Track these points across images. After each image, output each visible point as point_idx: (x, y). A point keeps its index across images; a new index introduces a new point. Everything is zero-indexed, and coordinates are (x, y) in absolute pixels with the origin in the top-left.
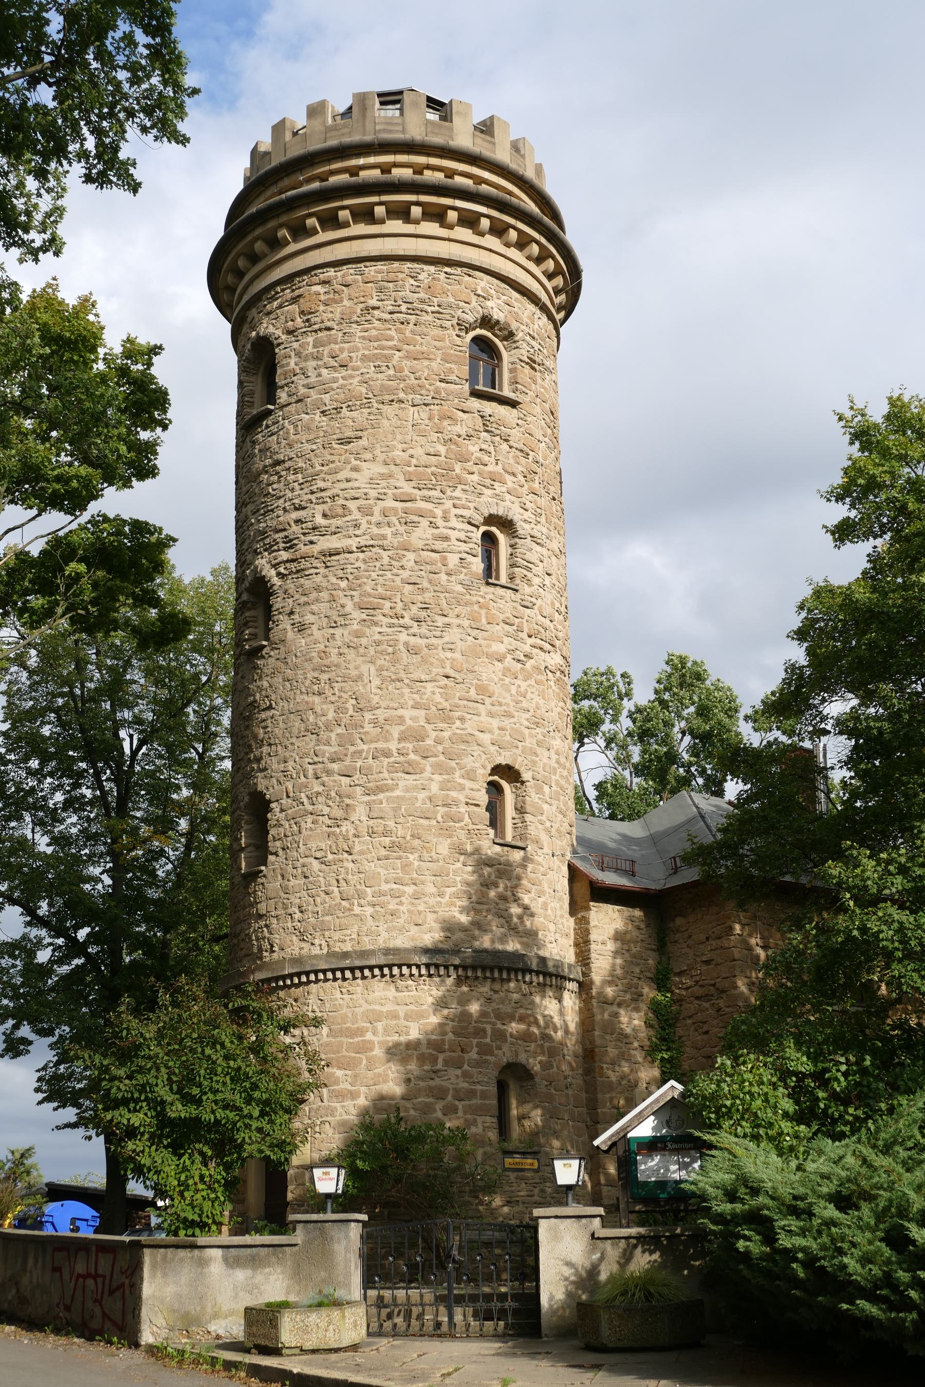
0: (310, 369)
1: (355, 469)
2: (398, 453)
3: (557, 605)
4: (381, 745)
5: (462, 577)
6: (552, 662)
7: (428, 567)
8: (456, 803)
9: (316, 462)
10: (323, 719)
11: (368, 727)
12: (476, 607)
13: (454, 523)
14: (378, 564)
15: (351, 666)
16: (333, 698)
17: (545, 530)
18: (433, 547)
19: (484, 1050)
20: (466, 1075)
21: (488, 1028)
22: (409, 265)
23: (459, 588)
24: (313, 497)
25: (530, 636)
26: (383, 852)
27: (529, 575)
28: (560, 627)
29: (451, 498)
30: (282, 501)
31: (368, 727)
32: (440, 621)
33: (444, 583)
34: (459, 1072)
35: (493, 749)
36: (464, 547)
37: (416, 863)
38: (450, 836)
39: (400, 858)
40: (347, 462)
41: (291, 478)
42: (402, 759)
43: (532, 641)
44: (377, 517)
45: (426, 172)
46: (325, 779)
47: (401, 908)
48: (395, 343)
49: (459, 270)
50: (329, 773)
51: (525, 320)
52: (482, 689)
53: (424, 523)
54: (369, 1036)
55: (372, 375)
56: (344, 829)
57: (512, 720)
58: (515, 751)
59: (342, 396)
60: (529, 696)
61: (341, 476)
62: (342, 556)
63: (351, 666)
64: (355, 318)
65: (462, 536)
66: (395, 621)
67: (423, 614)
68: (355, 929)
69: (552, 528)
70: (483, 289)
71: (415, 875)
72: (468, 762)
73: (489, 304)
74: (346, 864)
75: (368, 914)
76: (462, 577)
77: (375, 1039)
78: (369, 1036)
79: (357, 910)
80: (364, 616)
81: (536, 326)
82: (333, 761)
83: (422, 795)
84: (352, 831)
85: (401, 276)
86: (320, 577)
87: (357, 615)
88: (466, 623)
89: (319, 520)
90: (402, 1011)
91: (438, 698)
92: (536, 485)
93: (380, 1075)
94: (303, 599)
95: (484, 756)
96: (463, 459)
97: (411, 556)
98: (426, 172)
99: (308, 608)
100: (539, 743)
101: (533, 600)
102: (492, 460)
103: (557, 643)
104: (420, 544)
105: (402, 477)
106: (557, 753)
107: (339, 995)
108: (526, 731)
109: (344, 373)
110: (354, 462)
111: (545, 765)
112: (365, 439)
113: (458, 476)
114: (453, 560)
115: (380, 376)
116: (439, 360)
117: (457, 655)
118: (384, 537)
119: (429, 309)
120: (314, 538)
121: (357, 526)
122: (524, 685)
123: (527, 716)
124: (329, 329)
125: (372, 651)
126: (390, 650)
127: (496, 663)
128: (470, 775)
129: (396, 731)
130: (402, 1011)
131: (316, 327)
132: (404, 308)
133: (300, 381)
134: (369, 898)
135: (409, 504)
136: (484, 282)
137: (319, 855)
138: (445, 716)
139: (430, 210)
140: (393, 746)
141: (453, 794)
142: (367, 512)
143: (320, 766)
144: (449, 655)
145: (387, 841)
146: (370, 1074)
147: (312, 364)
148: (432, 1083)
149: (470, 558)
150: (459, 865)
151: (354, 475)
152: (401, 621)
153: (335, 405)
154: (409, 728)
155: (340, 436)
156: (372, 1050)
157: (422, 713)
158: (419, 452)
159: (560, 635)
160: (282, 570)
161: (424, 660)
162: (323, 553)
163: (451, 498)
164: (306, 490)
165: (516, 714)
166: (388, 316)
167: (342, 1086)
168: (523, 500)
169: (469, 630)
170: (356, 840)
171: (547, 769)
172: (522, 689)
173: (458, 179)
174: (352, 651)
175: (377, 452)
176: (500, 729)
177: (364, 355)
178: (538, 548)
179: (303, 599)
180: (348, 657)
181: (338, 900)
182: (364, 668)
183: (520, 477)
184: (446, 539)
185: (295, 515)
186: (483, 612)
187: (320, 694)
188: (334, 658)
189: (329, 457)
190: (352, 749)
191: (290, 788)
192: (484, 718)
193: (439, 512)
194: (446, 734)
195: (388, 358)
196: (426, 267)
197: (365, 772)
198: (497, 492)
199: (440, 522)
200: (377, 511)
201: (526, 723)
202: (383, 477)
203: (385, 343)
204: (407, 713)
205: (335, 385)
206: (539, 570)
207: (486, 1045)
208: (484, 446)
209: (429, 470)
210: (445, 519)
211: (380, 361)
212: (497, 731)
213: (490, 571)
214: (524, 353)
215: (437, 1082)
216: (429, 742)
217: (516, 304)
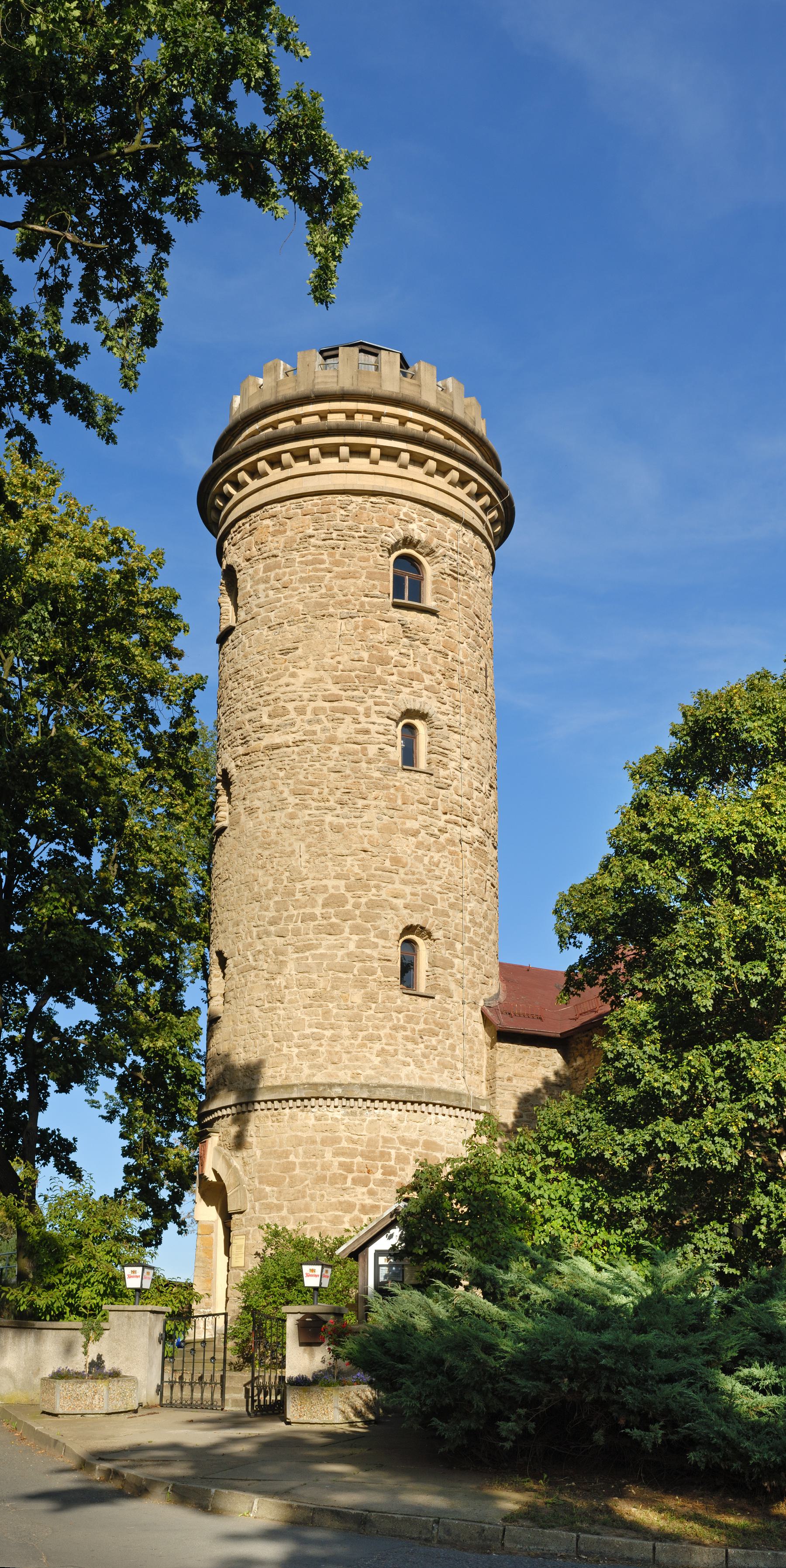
0: (261, 591)
1: (293, 675)
2: (327, 660)
3: (476, 784)
4: (308, 910)
5: (380, 764)
6: (469, 835)
7: (351, 757)
8: (371, 958)
9: (263, 670)
10: (265, 889)
11: (298, 896)
12: (392, 791)
13: (374, 718)
14: (309, 756)
15: (286, 844)
16: (272, 871)
17: (463, 720)
18: (355, 740)
19: (389, 1172)
20: (371, 1193)
21: (393, 1152)
22: (340, 497)
23: (377, 774)
24: (261, 700)
25: (445, 813)
26: (308, 1001)
27: (445, 760)
28: (478, 804)
29: (372, 697)
30: (239, 704)
31: (298, 896)
32: (361, 803)
33: (364, 771)
34: (365, 1190)
35: (405, 912)
36: (383, 738)
37: (335, 1011)
38: (365, 987)
39: (320, 1006)
40: (287, 669)
41: (246, 684)
42: (325, 922)
43: (448, 817)
44: (309, 716)
45: (357, 416)
46: (265, 939)
47: (321, 1049)
48: (327, 565)
49: (383, 499)
50: (268, 934)
51: (448, 537)
52: (396, 861)
53: (348, 719)
54: (292, 1158)
55: (307, 594)
56: (277, 982)
57: (424, 887)
58: (426, 913)
59: (284, 613)
60: (441, 865)
61: (282, 681)
62: (281, 750)
63: (286, 844)
64: (295, 546)
65: (381, 729)
66: (322, 804)
67: (346, 797)
68: (285, 1066)
69: (472, 718)
70: (405, 514)
71: (333, 1021)
72: (382, 924)
73: (411, 526)
74: (278, 1012)
75: (294, 1054)
76: (380, 764)
77: (297, 1161)
78: (292, 1158)
79: (285, 1050)
80: (297, 801)
81: (461, 542)
82: (271, 924)
83: (341, 953)
84: (284, 984)
85: (332, 507)
86: (266, 768)
87: (292, 800)
88: (383, 804)
89: (265, 720)
90: (318, 1137)
91: (356, 869)
92: (455, 681)
93: (299, 1191)
94: (253, 787)
95: (396, 919)
96: (384, 661)
97: (336, 748)
98: (357, 416)
99: (255, 794)
100: (451, 906)
101: (449, 782)
102: (411, 662)
103: (475, 818)
104: (344, 737)
105: (330, 681)
106: (471, 914)
107: (270, 1123)
108: (438, 896)
109: (287, 592)
110: (292, 670)
111: (456, 925)
112: (300, 650)
113: (379, 678)
114: (372, 750)
115: (314, 594)
116: (363, 578)
117: (374, 832)
118: (314, 733)
119: (356, 535)
120: (260, 735)
121: (293, 724)
122: (437, 857)
123: (440, 882)
124: (276, 556)
125: (303, 830)
126: (317, 829)
127: (410, 838)
128: (384, 935)
129: (320, 900)
130: (318, 1137)
131: (265, 555)
132: (334, 535)
133: (254, 602)
134: (296, 1040)
135: (335, 704)
136: (406, 507)
137: (259, 1003)
138: (361, 884)
139: (355, 449)
140: (318, 911)
141: (368, 951)
142: (301, 711)
143: (262, 928)
144: (367, 832)
145: (310, 992)
146: (292, 1190)
147: (262, 586)
148: (342, 1199)
149: (388, 748)
150: (372, 1012)
151: (292, 680)
152: (327, 804)
153: (279, 621)
154: (332, 895)
155: (281, 647)
156: (294, 1170)
157: (342, 883)
158: (344, 659)
159: (479, 811)
160: (239, 763)
161: (345, 837)
162: (267, 748)
163: (372, 697)
164: (257, 695)
165: (428, 881)
166: (321, 543)
167: (269, 1200)
168: (441, 695)
169: (385, 811)
170: (287, 991)
171: (460, 927)
172: (435, 860)
173: (386, 421)
174: (287, 830)
175: (310, 660)
176: (413, 894)
177: (301, 578)
178: (457, 736)
179: (253, 787)
180: (284, 836)
181: (271, 1042)
182: (296, 846)
183: (439, 676)
184: (367, 732)
185: (249, 716)
186: (399, 795)
187: (263, 867)
188: (273, 837)
189: (273, 666)
190: (285, 914)
191: (241, 947)
192: (397, 886)
193: (361, 709)
194: (363, 900)
195: (321, 579)
196: (354, 498)
197: (296, 933)
198: (415, 689)
199: (362, 718)
200: (309, 710)
201: (439, 889)
202: (315, 681)
203: (318, 566)
204: (330, 883)
205: (278, 604)
206: (457, 754)
207: (390, 1167)
208: (403, 651)
209: (353, 674)
210: (367, 715)
211: (314, 582)
212: (409, 897)
213: (409, 757)
214: (446, 565)
215: (346, 1198)
216: (349, 907)
217: (438, 525)
